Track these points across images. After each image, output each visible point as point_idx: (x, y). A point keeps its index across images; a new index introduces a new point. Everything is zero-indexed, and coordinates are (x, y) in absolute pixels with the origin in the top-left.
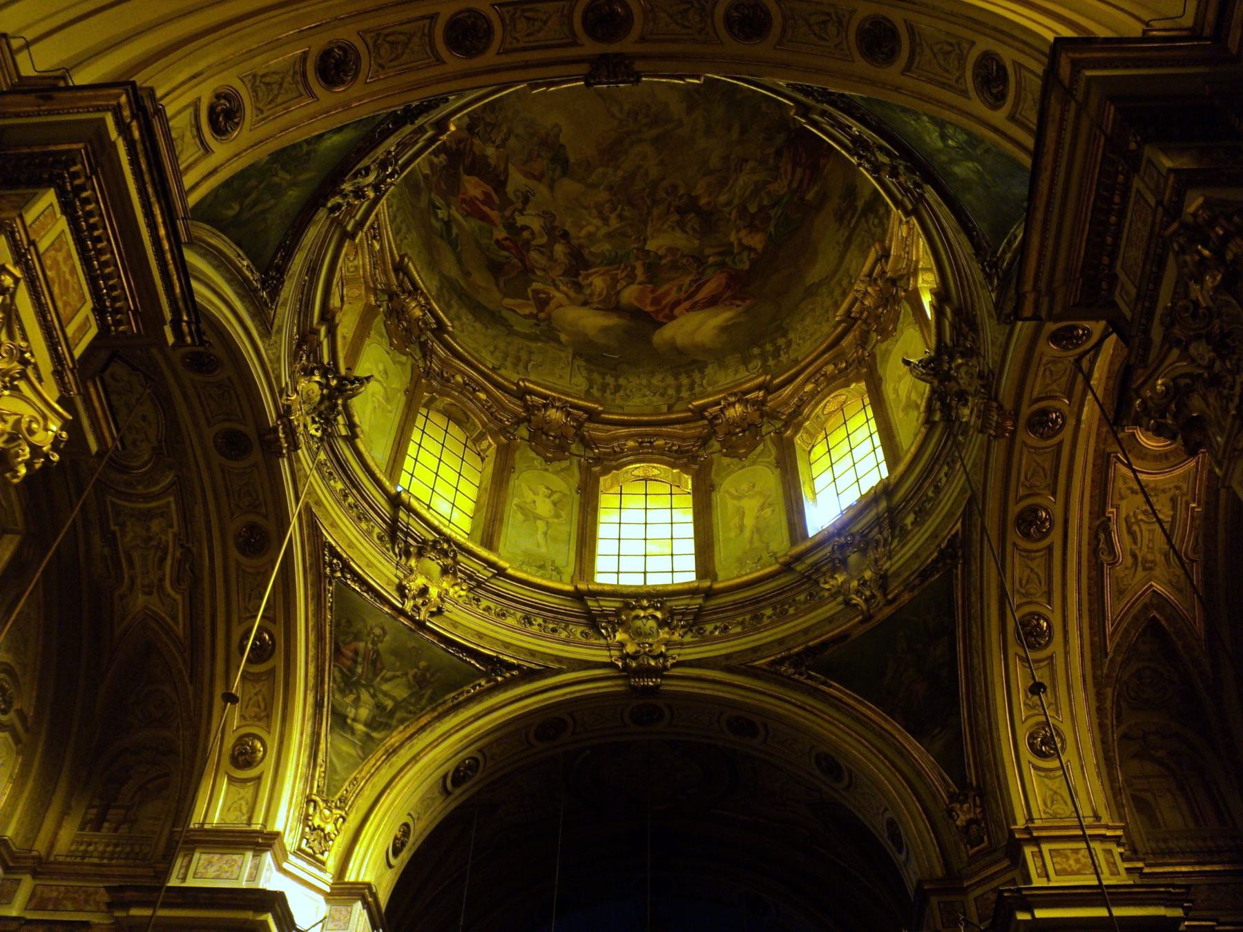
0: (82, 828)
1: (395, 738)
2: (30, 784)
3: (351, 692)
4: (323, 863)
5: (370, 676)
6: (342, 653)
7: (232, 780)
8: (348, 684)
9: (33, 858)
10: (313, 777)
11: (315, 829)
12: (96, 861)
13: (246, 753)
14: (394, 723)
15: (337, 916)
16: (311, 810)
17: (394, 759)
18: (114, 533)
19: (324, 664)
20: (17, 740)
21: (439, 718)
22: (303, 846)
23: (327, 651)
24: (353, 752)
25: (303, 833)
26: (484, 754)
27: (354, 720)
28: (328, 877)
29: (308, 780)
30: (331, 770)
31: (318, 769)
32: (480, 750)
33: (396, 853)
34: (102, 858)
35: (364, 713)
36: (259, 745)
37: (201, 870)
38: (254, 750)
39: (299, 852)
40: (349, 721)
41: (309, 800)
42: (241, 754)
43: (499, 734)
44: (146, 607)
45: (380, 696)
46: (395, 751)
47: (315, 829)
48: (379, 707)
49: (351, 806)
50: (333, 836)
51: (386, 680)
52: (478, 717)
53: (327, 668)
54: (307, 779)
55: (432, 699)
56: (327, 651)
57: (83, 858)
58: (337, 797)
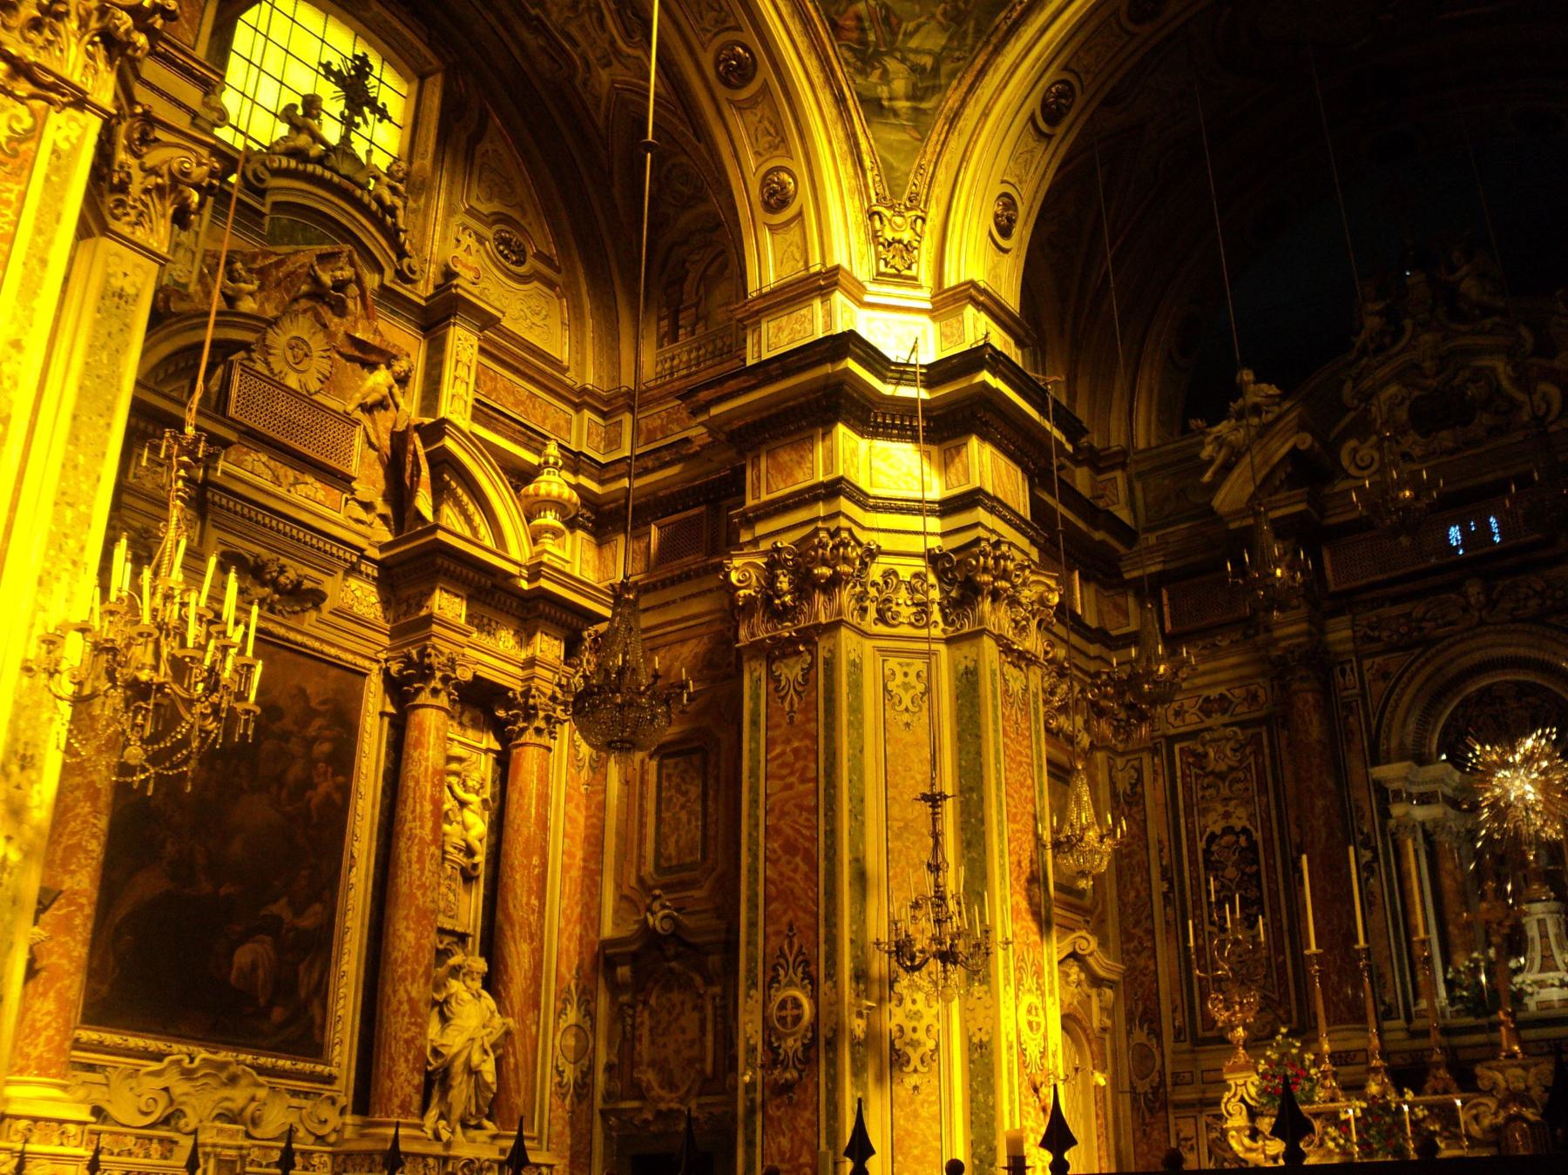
0: (660, 345)
1: (953, 100)
2: (590, 322)
3: (874, 68)
4: (915, 278)
5: (888, 37)
6: (842, 28)
7: (773, 229)
8: (865, 59)
9: (623, 395)
10: (866, 185)
11: (890, 244)
12: (684, 372)
13: (776, 192)
14: (943, 81)
15: (948, 331)
16: (877, 225)
17: (961, 123)
18: (537, 18)
19: (824, 49)
20: (551, 284)
21: (998, 50)
22: (883, 269)
23: (823, 34)
24: (905, 137)
25: (877, 253)
26: (1072, 71)
27: (891, 99)
28: (926, 293)
29: (863, 191)
30: (887, 171)
31: (869, 175)
32: (1065, 68)
33: (1005, 232)
34: (689, 367)
35: (899, 85)
36: (785, 177)
37: (773, 340)
38: (783, 186)
39: (879, 277)
40: (886, 103)
41: (871, 215)
42: (771, 195)
43: (1081, 36)
44: (613, 82)
45: (911, 56)
46: (957, 115)
47: (890, 244)
48: (916, 69)
49: (926, 202)
50: (915, 244)
51: (910, 35)
52: (1043, 31)
53: (831, 53)
54: (860, 193)
55: (978, 32)
56: (823, 34)
57: (672, 374)
58: (905, 197)
